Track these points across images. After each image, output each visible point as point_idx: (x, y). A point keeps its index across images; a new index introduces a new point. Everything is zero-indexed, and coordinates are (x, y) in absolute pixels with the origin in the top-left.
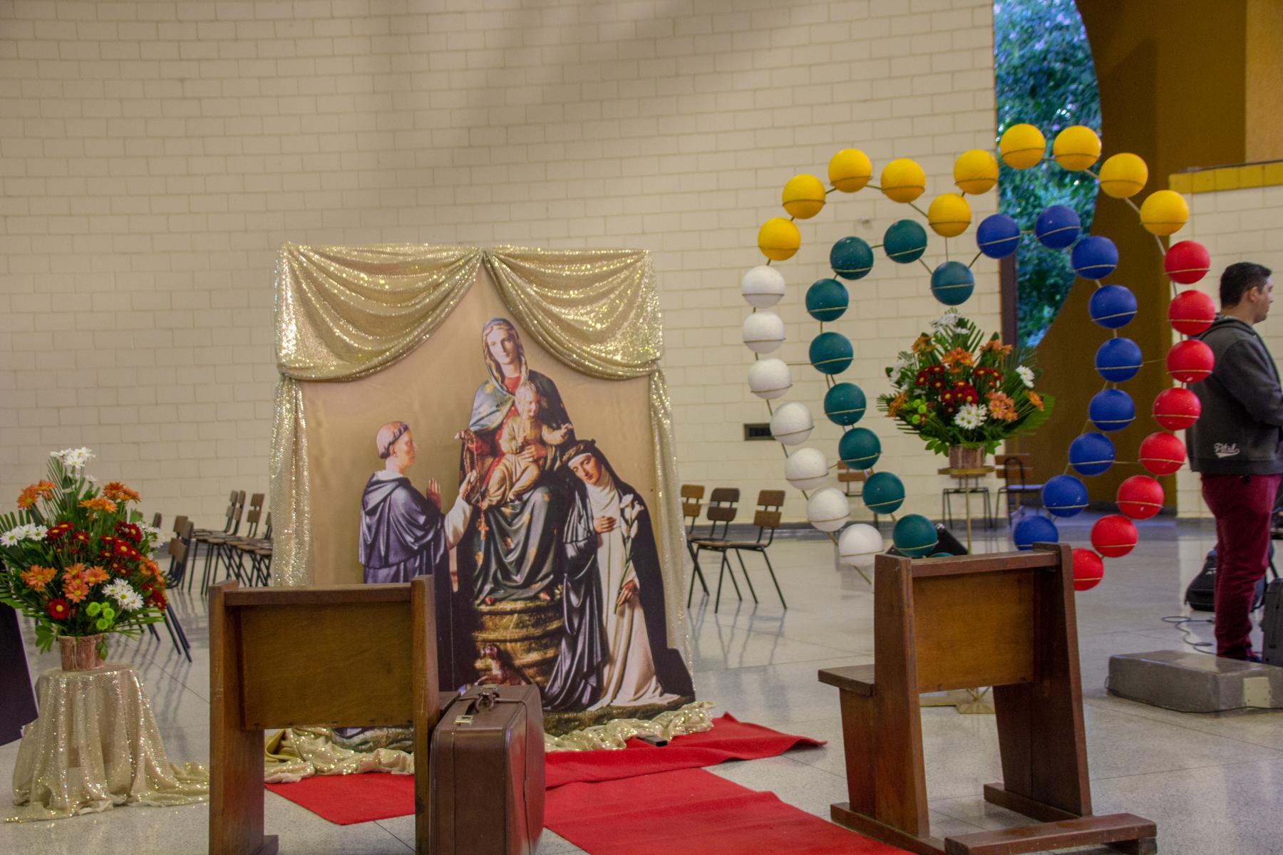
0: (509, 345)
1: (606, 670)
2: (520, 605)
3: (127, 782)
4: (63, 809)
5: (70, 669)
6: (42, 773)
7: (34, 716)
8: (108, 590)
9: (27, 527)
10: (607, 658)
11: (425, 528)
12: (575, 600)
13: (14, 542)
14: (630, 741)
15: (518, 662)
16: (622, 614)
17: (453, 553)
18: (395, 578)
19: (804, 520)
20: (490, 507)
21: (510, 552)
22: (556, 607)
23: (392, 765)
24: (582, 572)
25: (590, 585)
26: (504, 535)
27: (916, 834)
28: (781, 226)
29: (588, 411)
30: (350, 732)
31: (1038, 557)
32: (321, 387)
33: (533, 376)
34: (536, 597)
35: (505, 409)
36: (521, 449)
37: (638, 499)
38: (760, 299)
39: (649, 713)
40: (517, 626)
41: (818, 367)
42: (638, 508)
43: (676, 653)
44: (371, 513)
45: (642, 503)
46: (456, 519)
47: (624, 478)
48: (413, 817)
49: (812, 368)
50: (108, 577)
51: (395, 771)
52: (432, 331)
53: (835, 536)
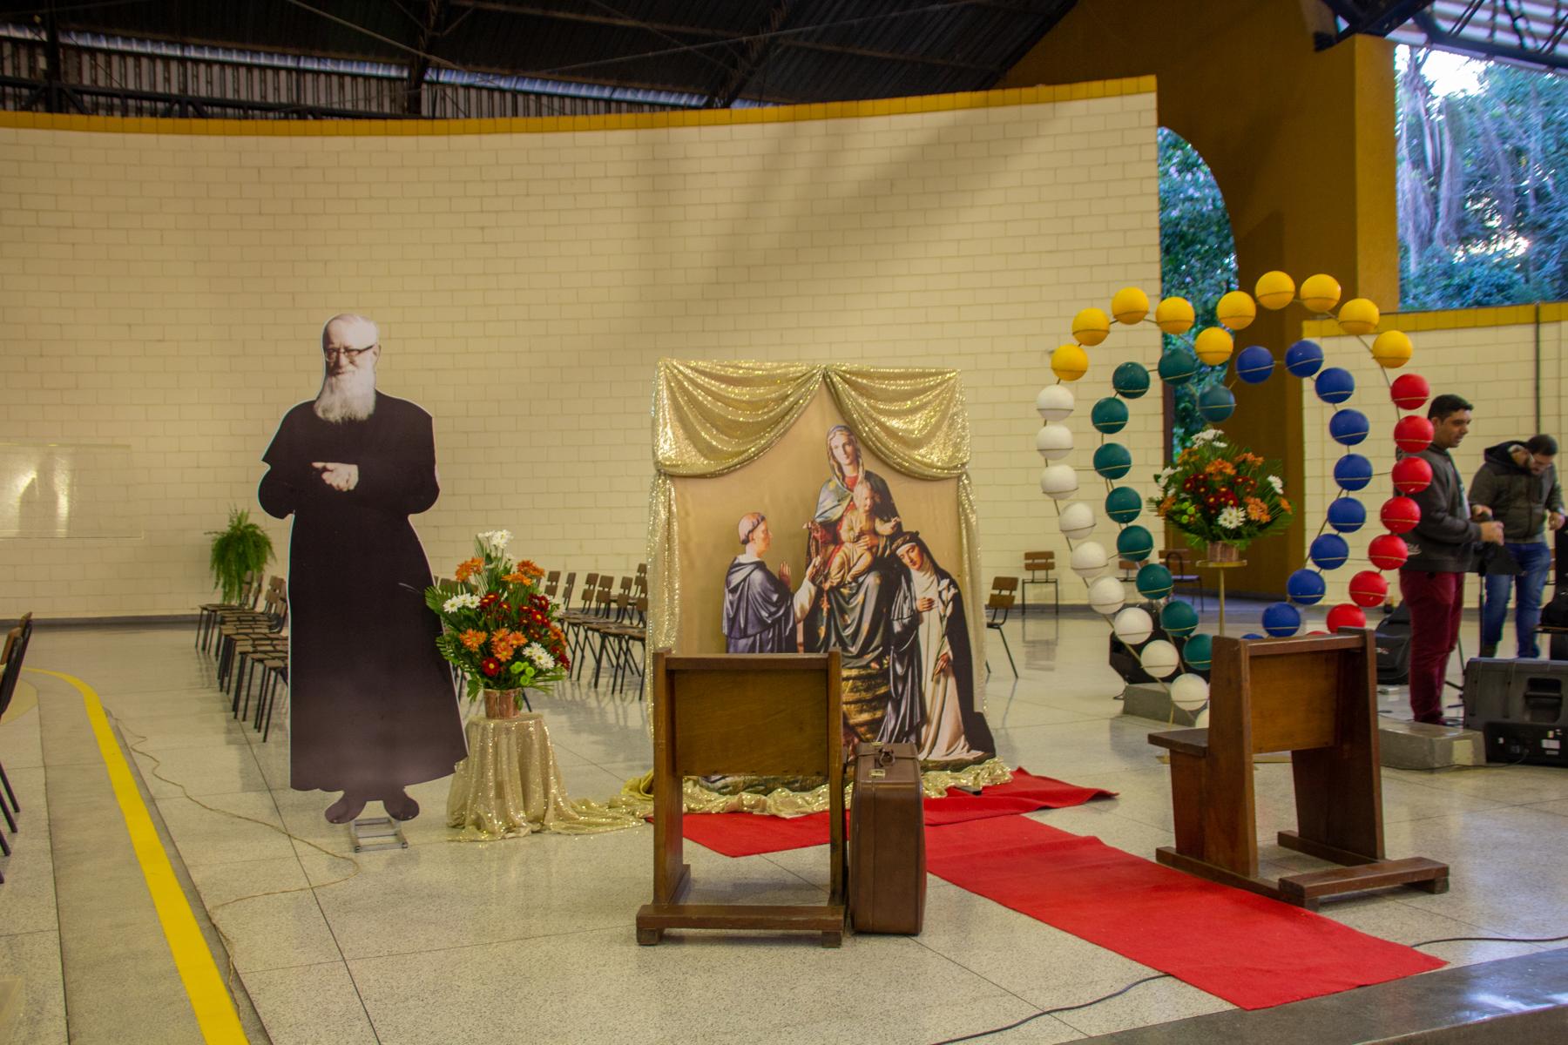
0: (849, 448)
1: (924, 730)
2: (854, 673)
3: (541, 813)
4: (492, 833)
5: (494, 717)
6: (474, 802)
7: (463, 755)
8: (527, 652)
9: (461, 598)
10: (925, 719)
11: (778, 605)
12: (899, 669)
13: (455, 609)
14: (950, 790)
15: (852, 721)
16: (938, 682)
17: (800, 627)
18: (752, 649)
19: (1085, 602)
20: (832, 588)
21: (847, 626)
22: (884, 674)
23: (753, 807)
24: (906, 646)
25: (912, 656)
26: (843, 612)
27: (1248, 874)
28: (1070, 351)
29: (917, 509)
30: (714, 778)
31: (1346, 639)
32: (690, 481)
33: (869, 476)
34: (867, 666)
35: (845, 504)
36: (858, 538)
37: (953, 583)
38: (1051, 414)
39: (958, 766)
40: (852, 690)
41: (1102, 473)
42: (953, 591)
43: (981, 716)
44: (733, 591)
45: (956, 586)
46: (803, 598)
47: (942, 565)
48: (828, 846)
49: (1096, 474)
50: (525, 641)
51: (756, 812)
52: (783, 435)
53: (1111, 618)
